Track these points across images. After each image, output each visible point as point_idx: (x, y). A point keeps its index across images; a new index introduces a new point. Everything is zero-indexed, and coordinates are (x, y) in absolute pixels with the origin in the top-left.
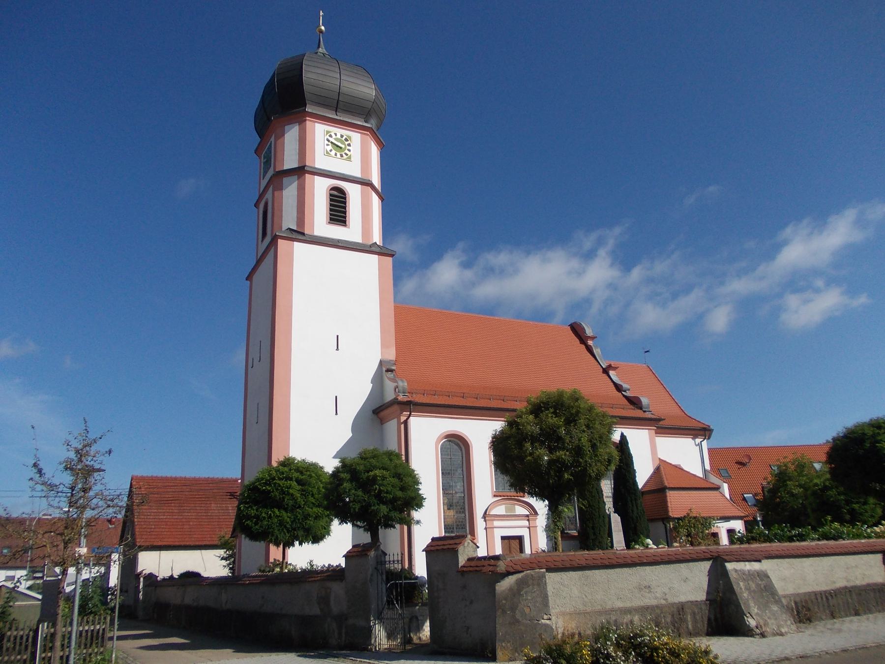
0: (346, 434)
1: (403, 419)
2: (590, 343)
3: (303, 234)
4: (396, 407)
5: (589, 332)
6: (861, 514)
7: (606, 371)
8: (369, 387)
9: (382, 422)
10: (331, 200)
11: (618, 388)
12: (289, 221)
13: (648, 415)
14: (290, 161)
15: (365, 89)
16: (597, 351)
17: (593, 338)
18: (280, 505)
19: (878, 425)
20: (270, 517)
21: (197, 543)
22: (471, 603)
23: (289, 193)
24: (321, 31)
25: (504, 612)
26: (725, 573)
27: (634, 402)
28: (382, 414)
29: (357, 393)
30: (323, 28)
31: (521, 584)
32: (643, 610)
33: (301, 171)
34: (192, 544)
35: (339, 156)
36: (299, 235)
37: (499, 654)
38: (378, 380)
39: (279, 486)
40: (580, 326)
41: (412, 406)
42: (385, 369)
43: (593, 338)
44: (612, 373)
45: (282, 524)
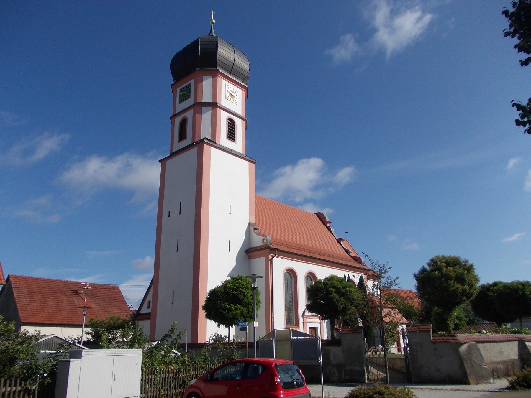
0: (233, 264)
1: (270, 258)
2: (328, 225)
3: (215, 143)
4: (268, 251)
5: (327, 219)
6: (460, 325)
7: (339, 241)
8: (243, 237)
9: (250, 258)
10: (229, 126)
11: (347, 251)
12: (205, 133)
13: (364, 267)
14: (206, 98)
15: (244, 64)
16: (332, 230)
17: (329, 222)
18: (240, 302)
19: (525, 285)
20: (236, 309)
21: (60, 323)
22: (441, 357)
23: (206, 117)
24: (212, 23)
25: (467, 362)
26: (526, 347)
27: (357, 259)
28: (250, 254)
29: (238, 241)
30: (214, 21)
31: (469, 347)
32: (503, 362)
33: (214, 105)
34: (57, 323)
35: (232, 101)
36: (213, 142)
37: (471, 381)
38: (248, 233)
39: (243, 292)
40: (322, 215)
41: (272, 250)
42: (252, 229)
43: (329, 222)
44: (342, 243)
45: (242, 313)
